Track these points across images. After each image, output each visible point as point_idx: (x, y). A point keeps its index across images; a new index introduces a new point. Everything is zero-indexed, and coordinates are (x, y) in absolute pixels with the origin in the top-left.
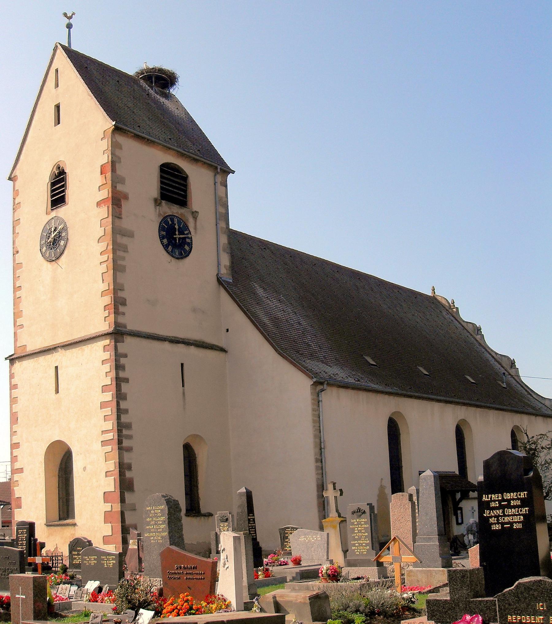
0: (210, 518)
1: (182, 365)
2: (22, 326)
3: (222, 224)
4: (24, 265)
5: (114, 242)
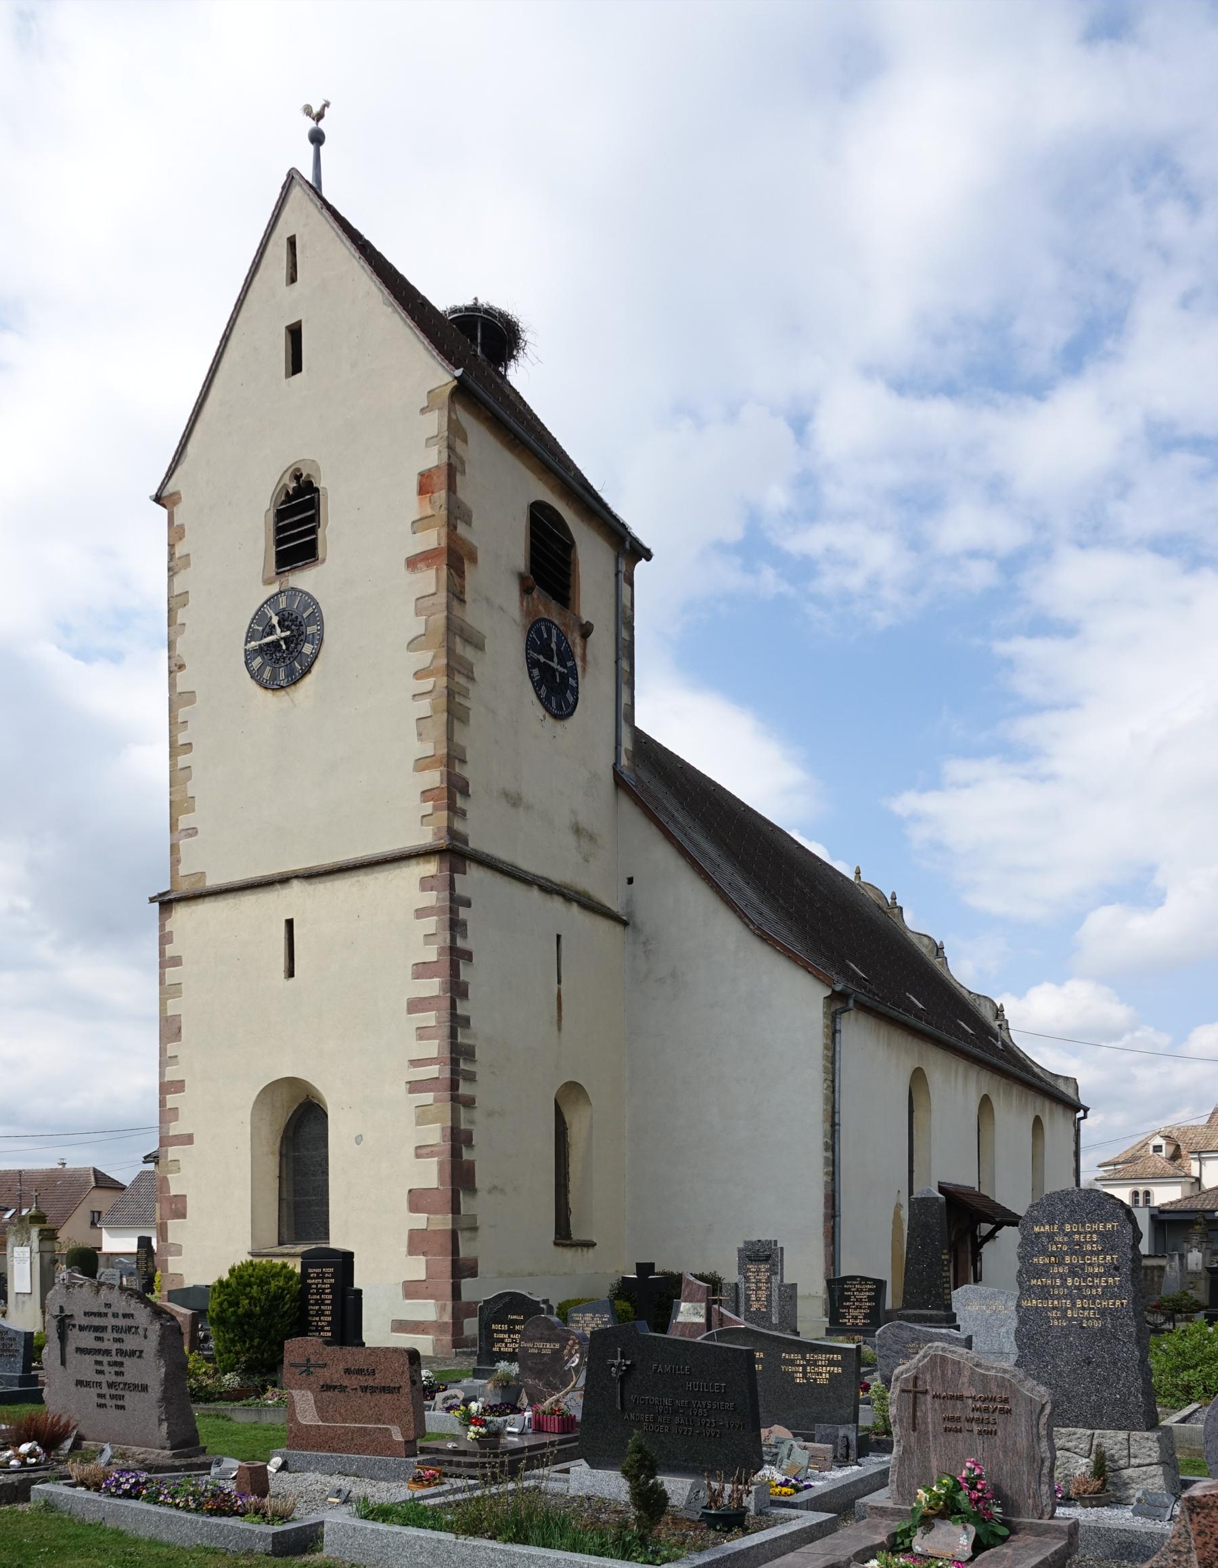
0: (591, 1251)
1: (559, 937)
2: (192, 832)
3: (624, 665)
4: (199, 697)
5: (450, 652)
